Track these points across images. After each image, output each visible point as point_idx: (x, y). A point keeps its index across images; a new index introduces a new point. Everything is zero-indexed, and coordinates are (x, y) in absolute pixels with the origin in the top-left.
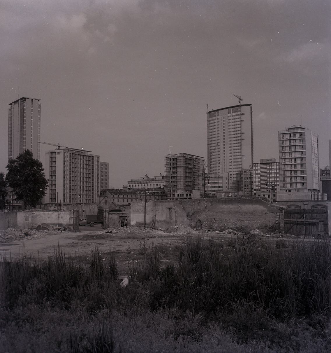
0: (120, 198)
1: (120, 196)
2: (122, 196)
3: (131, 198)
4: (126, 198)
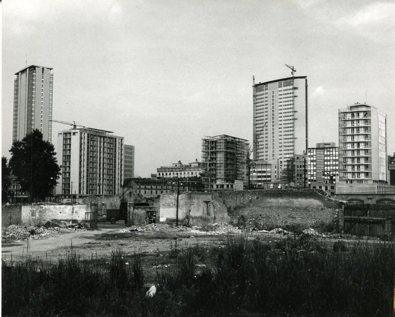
0: (147, 189)
1: (147, 187)
2: (150, 187)
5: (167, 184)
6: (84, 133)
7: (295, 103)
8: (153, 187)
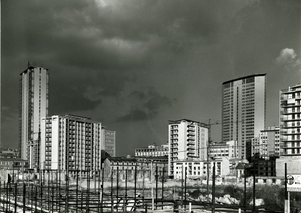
0: (119, 165)
1: (119, 164)
2: (122, 164)
3: (131, 166)
4: (121, 165)
5: (137, 161)
6: (63, 119)
7: (52, 125)
8: (125, 164)
